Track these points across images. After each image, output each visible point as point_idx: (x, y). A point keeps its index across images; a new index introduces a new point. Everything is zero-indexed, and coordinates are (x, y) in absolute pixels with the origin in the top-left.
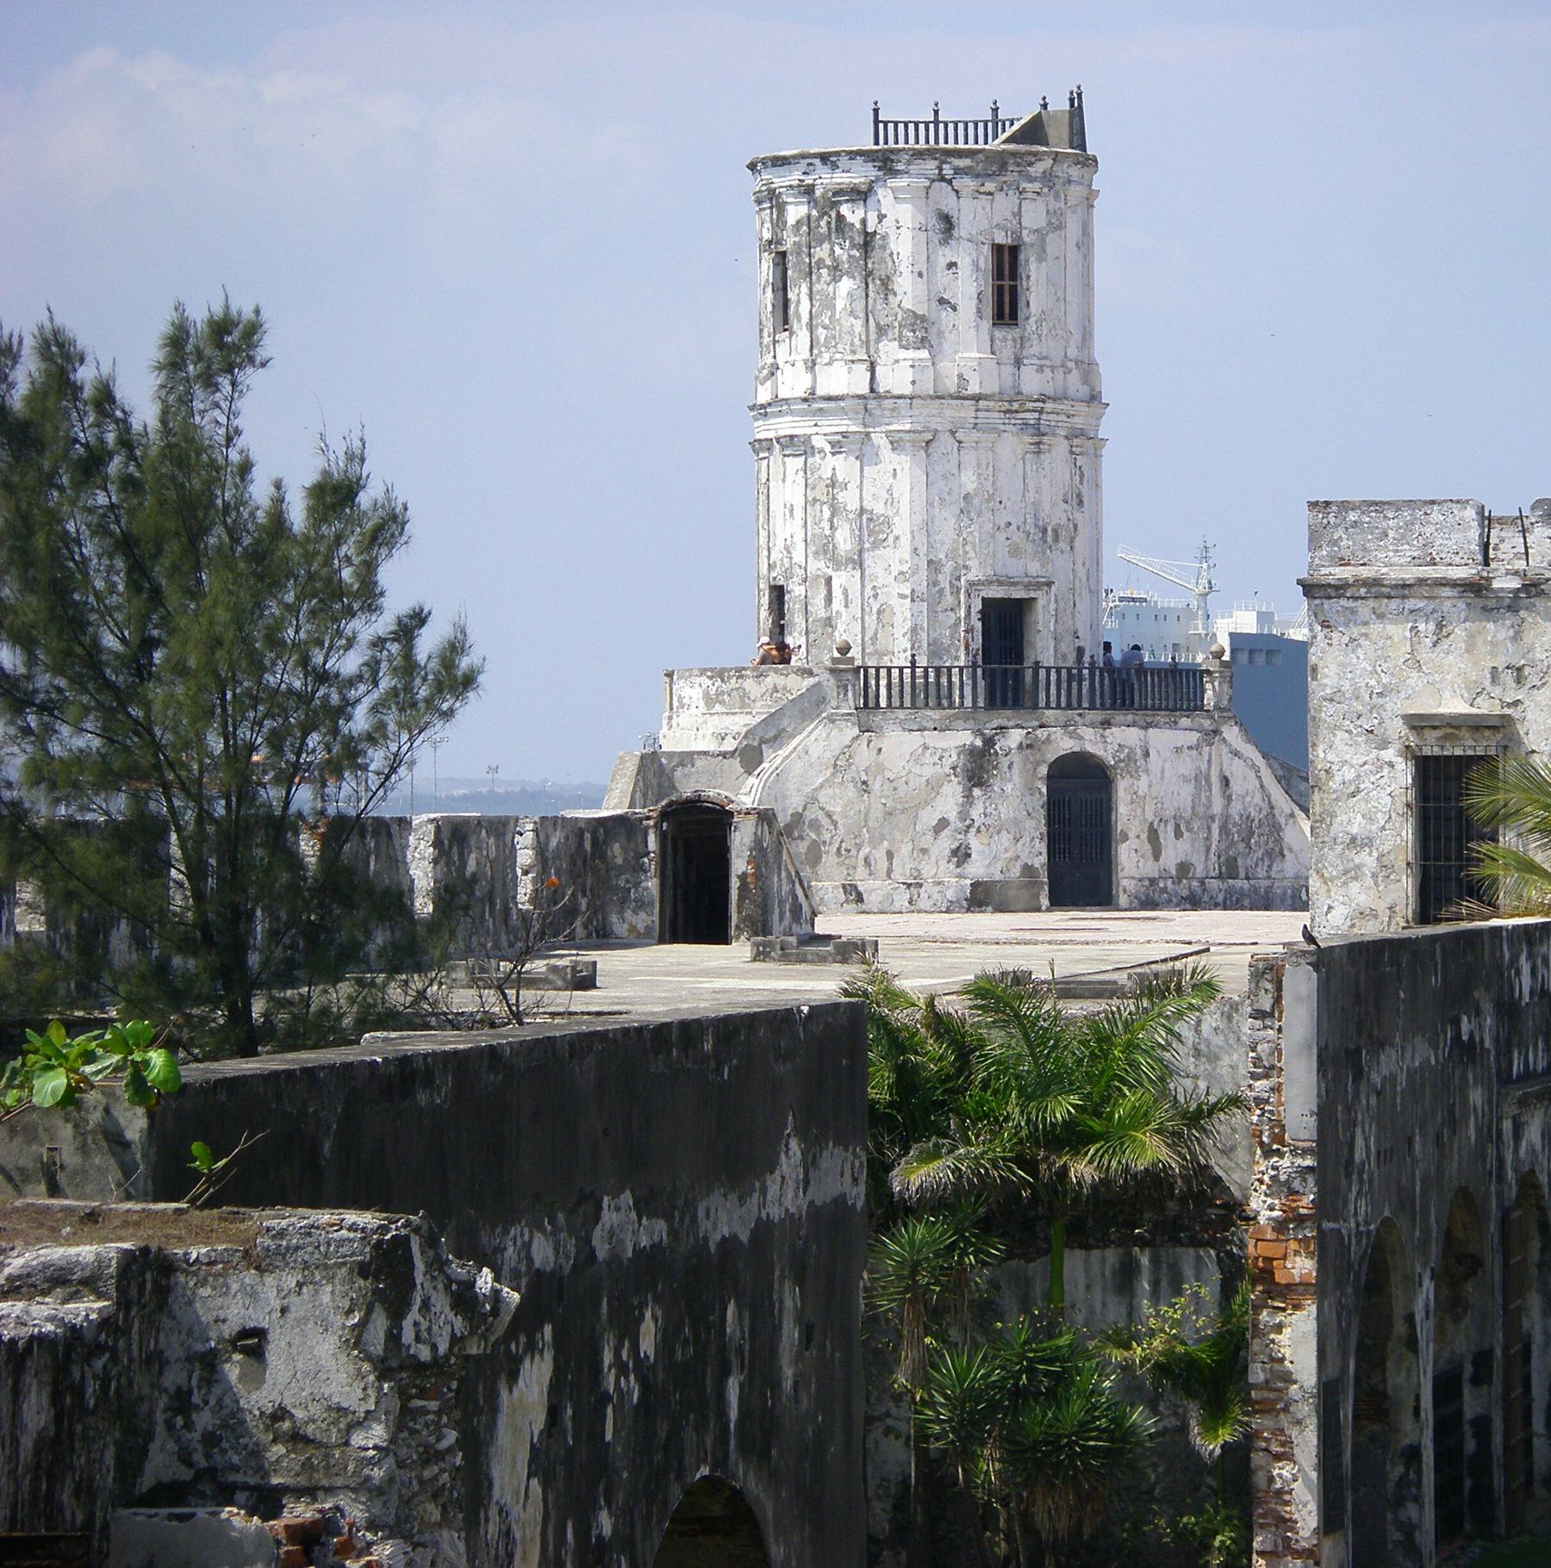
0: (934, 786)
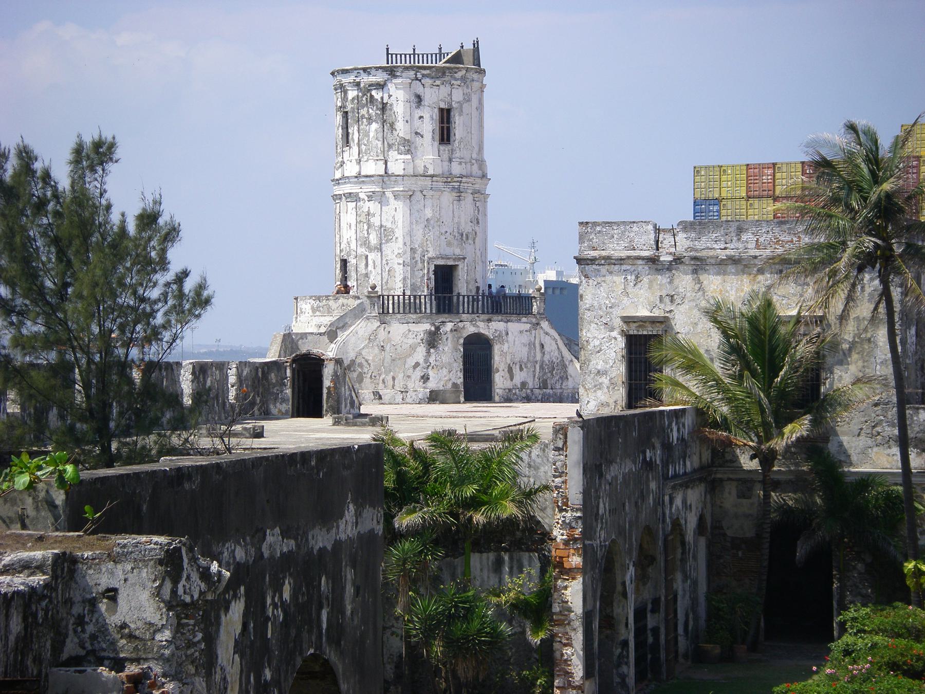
0: (413, 348)
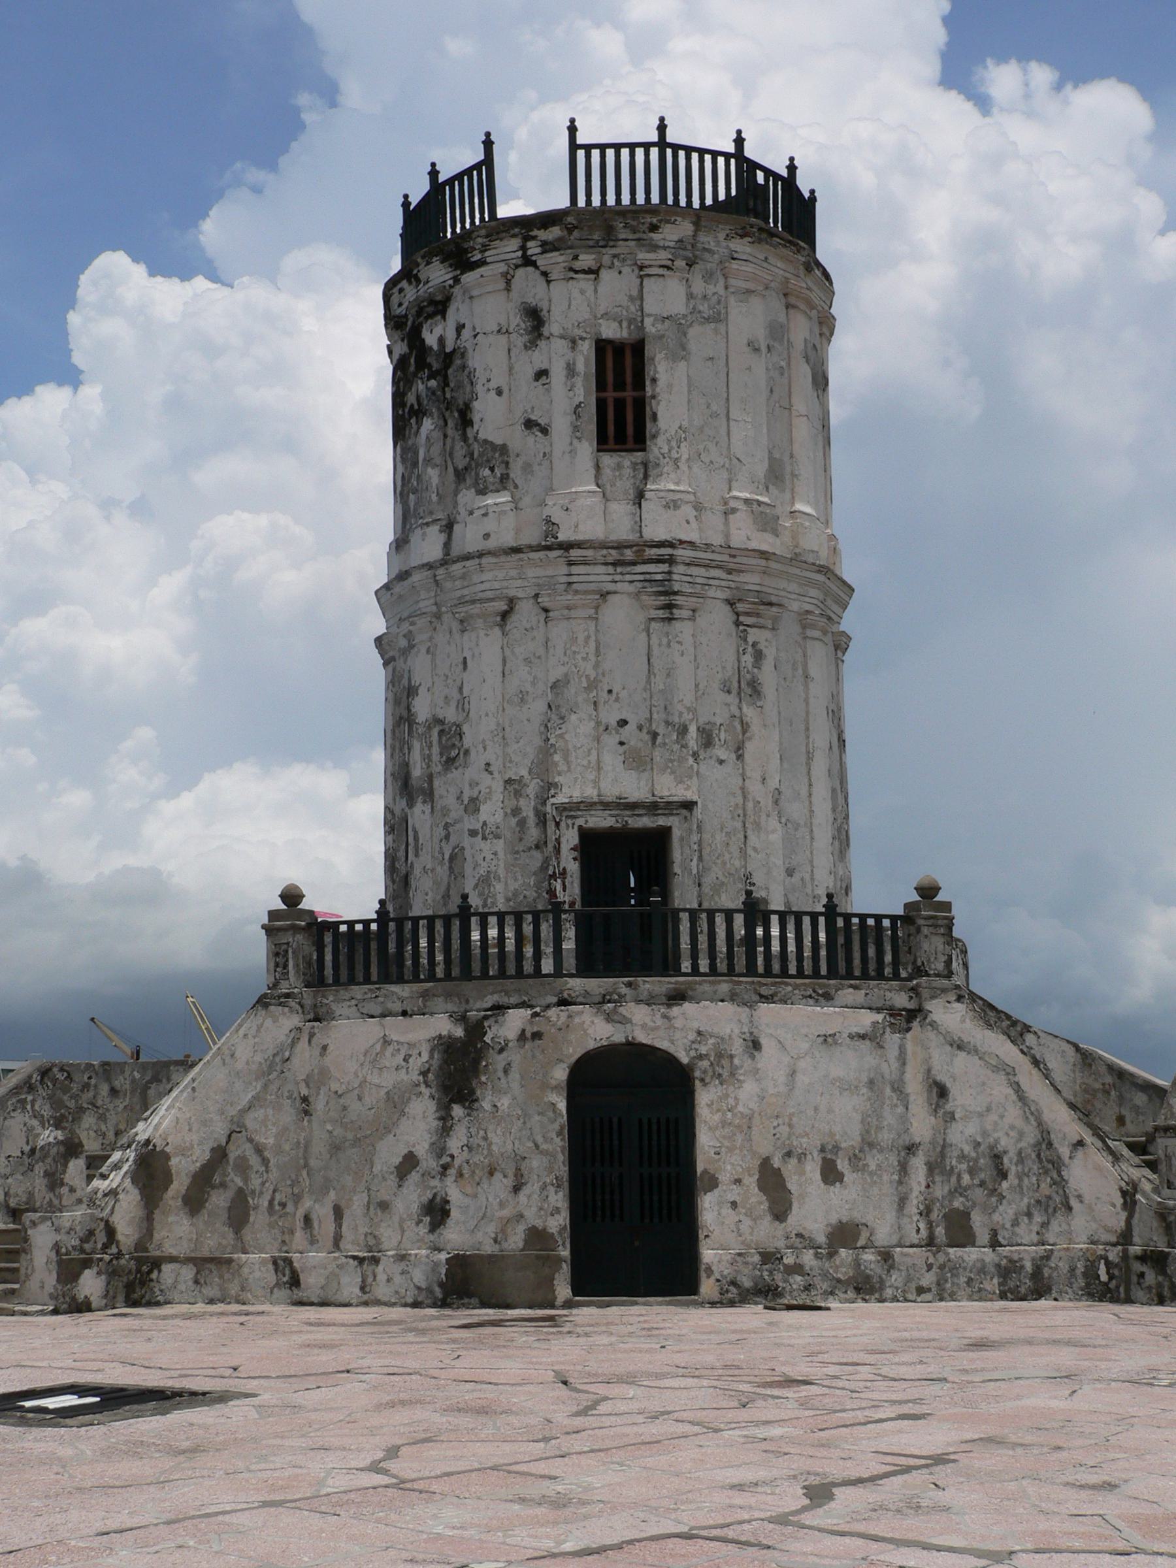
0: (396, 1103)
